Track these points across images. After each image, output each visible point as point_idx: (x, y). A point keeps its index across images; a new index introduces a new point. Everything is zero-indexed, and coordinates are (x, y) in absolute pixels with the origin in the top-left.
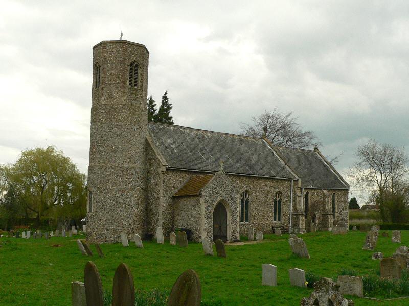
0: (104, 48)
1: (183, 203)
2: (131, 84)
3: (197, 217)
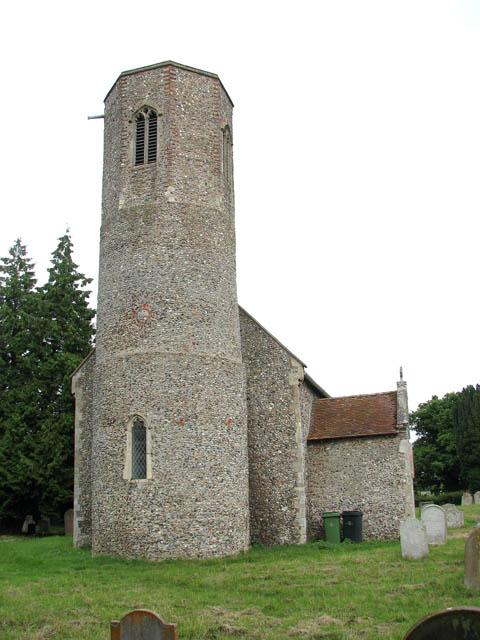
0: (171, 76)
1: (335, 452)
2: (139, 160)
3: (391, 484)
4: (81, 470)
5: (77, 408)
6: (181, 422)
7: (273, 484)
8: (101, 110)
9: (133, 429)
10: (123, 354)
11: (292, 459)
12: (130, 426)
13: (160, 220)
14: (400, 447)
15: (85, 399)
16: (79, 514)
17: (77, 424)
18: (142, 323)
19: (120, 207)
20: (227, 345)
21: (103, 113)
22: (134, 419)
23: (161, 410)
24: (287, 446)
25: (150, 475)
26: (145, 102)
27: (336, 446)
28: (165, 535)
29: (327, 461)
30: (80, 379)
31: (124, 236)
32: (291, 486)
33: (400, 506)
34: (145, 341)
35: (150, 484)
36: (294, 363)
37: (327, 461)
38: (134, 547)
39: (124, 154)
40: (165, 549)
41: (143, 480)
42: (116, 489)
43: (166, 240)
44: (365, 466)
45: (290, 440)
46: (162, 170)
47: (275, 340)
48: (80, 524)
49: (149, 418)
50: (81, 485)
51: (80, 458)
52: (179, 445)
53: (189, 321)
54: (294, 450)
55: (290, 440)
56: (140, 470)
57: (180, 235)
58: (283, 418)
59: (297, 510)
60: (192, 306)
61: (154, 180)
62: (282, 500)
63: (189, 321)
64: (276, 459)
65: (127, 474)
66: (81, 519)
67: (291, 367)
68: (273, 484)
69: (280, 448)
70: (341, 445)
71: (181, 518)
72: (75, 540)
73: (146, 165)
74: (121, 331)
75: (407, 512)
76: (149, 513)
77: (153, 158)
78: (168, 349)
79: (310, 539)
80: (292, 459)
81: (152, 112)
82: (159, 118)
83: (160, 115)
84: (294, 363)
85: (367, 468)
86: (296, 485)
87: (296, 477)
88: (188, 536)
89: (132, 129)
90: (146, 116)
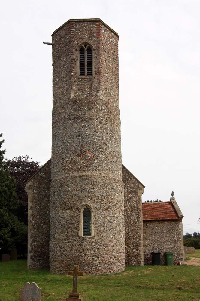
1: (151, 226)
2: (82, 73)
3: (175, 241)
4: (31, 230)
5: (28, 200)
6: (106, 210)
7: (129, 239)
8: (50, 41)
9: (84, 212)
10: (76, 174)
11: (138, 229)
12: (82, 210)
13: (96, 108)
14: (179, 226)
15: (33, 196)
16: (30, 252)
17: (29, 208)
18: (88, 160)
19: (72, 97)
20: (119, 176)
21: (51, 42)
22: (85, 207)
23: (98, 203)
24: (136, 223)
25: (93, 234)
26: (85, 40)
27: (152, 224)
28: (99, 263)
29: (147, 230)
30: (30, 185)
31: (75, 113)
32: (137, 240)
33: (179, 250)
34: (89, 169)
35: (93, 238)
36: (140, 185)
37: (147, 230)
38: (85, 268)
39: (73, 68)
40: (100, 269)
41: (89, 236)
42: (75, 241)
43: (99, 119)
44: (164, 233)
45: (138, 220)
46: (96, 82)
47: (132, 175)
48: (31, 257)
49: (92, 206)
50: (31, 238)
51: (31, 224)
52: (106, 220)
53: (109, 161)
54: (139, 225)
55: (138, 220)
56: (87, 232)
57: (105, 118)
58: (135, 210)
59: (140, 251)
60: (110, 154)
61: (91, 85)
62: (133, 246)
63: (109, 161)
64: (131, 228)
65: (81, 233)
66: (32, 254)
67: (139, 187)
68: (129, 239)
69: (133, 223)
70: (162, 224)
71: (107, 254)
72: (29, 264)
73: (86, 76)
74: (75, 163)
75: (181, 253)
76: (93, 252)
77: (90, 73)
78: (101, 174)
79: (144, 265)
80: (138, 229)
81: (89, 47)
82: (93, 52)
83: (94, 50)
84: (140, 185)
85: (165, 234)
86: (140, 240)
87: (140, 236)
88: (110, 263)
89: (77, 54)
90: (86, 49)
